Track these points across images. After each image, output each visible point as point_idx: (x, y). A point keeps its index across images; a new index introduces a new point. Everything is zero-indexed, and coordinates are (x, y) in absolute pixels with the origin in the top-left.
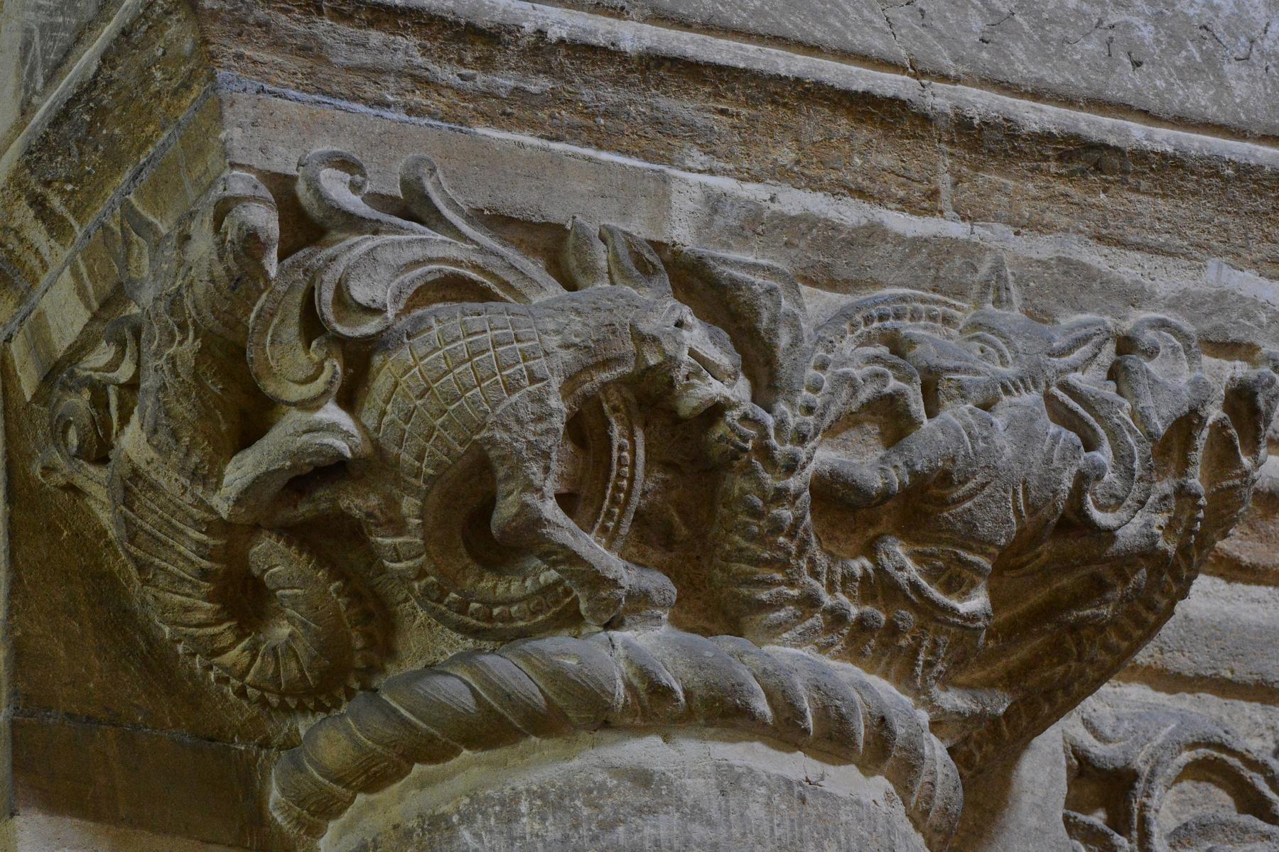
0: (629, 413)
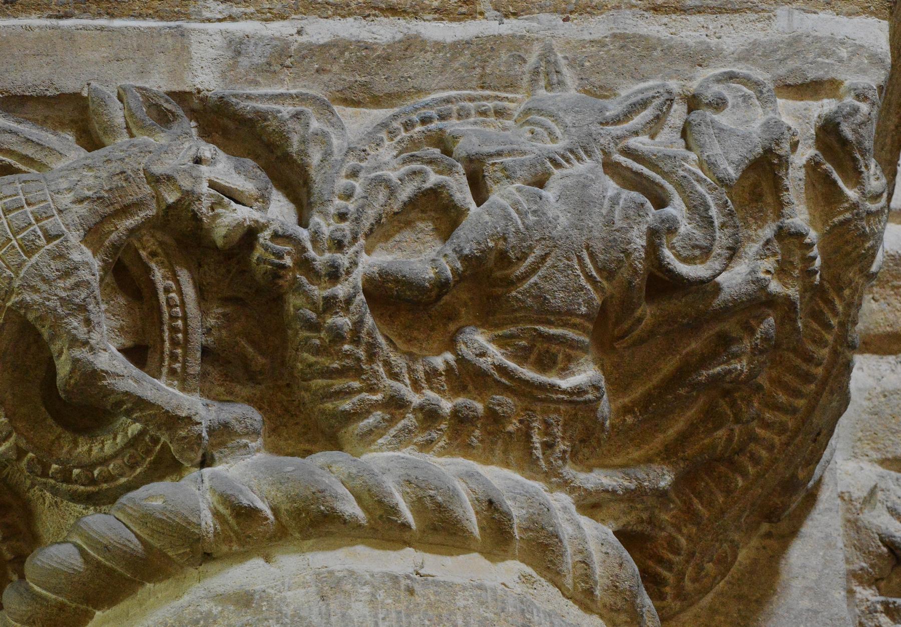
0: (167, 255)
